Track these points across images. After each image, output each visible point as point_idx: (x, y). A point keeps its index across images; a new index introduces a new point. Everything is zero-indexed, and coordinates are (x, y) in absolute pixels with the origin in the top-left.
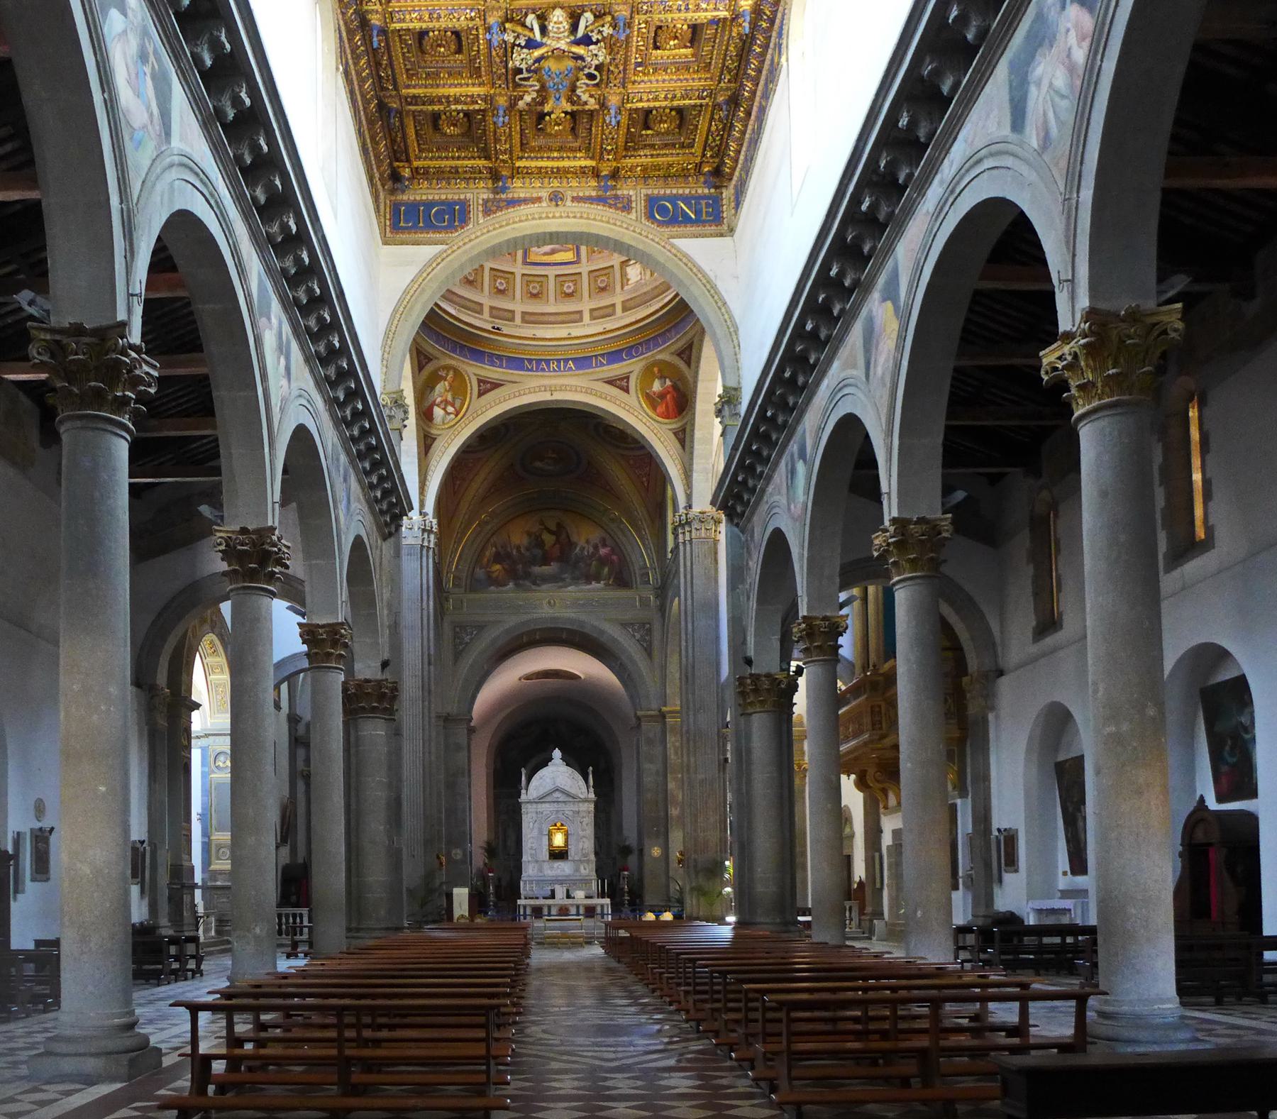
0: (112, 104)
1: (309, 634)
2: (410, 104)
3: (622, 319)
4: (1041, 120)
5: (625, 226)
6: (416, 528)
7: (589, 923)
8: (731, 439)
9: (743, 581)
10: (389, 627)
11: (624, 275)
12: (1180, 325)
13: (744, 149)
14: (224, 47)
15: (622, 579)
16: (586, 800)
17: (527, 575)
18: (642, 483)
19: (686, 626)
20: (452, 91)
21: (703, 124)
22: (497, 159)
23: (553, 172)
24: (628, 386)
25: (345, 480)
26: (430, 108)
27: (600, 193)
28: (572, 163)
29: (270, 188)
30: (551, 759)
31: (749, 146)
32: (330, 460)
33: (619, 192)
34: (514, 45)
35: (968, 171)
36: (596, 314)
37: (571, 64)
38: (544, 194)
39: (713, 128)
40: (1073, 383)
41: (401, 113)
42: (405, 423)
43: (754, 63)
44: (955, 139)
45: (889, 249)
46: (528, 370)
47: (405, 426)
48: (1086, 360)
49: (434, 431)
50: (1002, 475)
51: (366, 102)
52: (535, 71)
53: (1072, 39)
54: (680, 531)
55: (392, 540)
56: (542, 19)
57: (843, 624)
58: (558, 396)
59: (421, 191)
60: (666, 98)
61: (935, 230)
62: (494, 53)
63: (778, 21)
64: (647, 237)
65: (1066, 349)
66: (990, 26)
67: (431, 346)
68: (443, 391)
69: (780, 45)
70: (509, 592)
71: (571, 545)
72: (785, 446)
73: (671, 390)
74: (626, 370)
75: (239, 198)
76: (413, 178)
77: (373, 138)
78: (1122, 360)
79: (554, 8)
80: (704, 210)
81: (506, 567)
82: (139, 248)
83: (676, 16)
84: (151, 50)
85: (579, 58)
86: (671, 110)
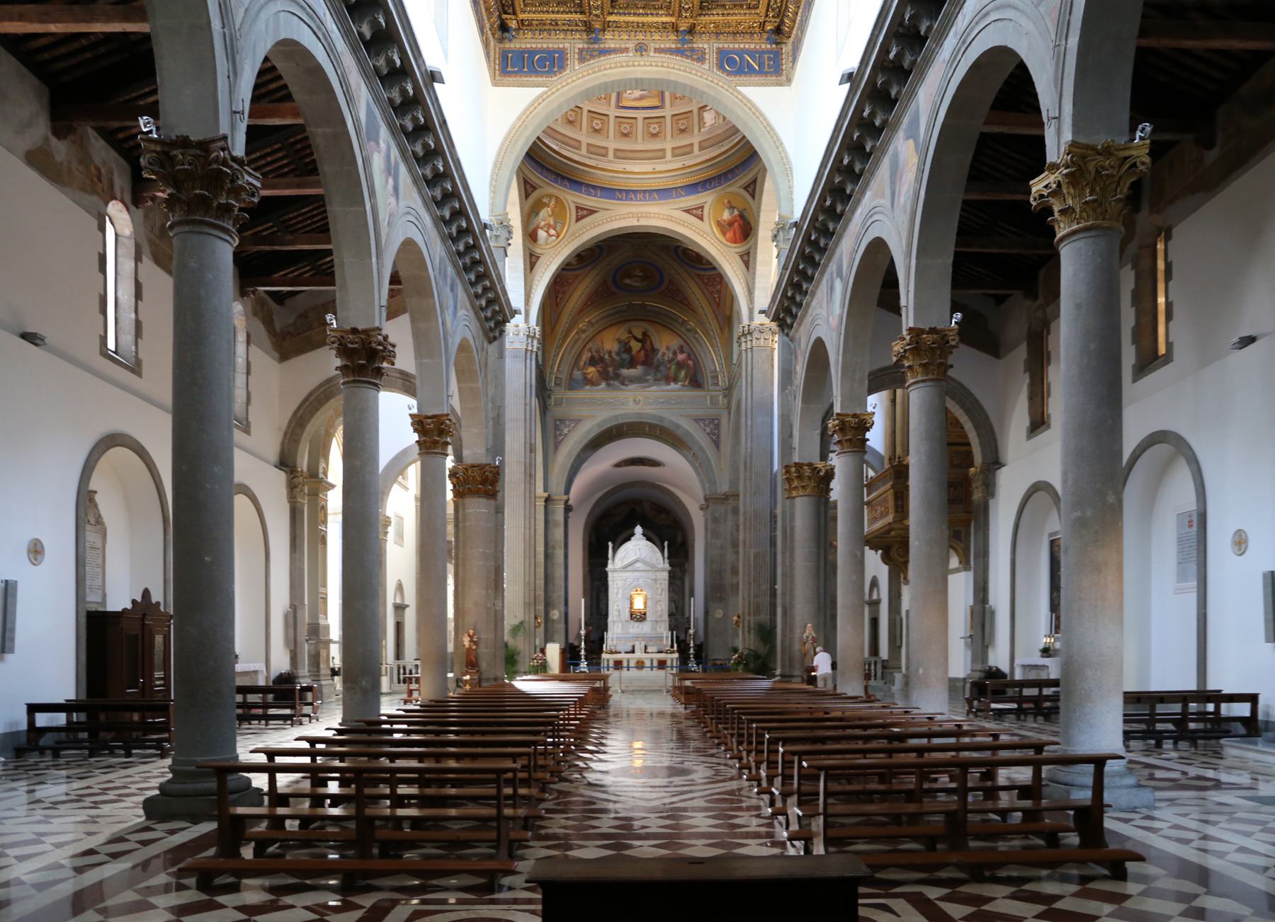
3: (699, 156)
5: (699, 74)
6: (522, 334)
7: (662, 673)
8: (783, 260)
10: (493, 419)
11: (701, 119)
12: (1147, 160)
15: (696, 382)
16: (663, 570)
17: (617, 376)
18: (714, 298)
19: (746, 422)
23: (638, 27)
24: (702, 215)
28: (655, 19)
29: (375, 24)
30: (633, 535)
31: (804, 9)
32: (437, 272)
33: (695, 45)
35: (977, 23)
38: (631, 45)
40: (1056, 209)
42: (510, 242)
45: (912, 93)
46: (619, 199)
47: (510, 244)
48: (1068, 188)
49: (538, 251)
50: (1007, 296)
54: (743, 339)
55: (496, 343)
57: (870, 421)
58: (643, 222)
59: (526, 40)
61: (950, 75)
64: (718, 84)
67: (535, 177)
68: (546, 215)
70: (601, 392)
71: (654, 350)
72: (826, 266)
73: (738, 218)
74: (703, 201)
75: (346, 33)
76: (520, 29)
78: (1098, 188)
80: (767, 63)
81: (600, 369)
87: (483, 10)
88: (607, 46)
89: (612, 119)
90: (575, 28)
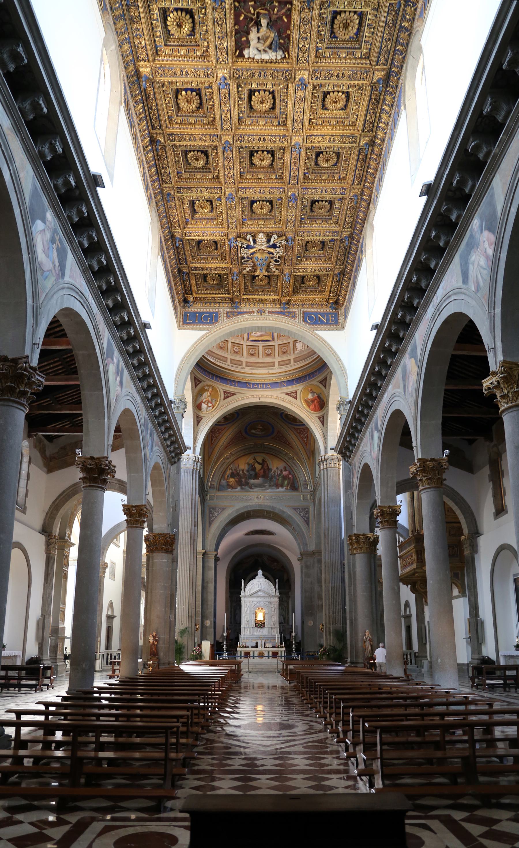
0: (33, 259)
1: (127, 510)
2: (193, 270)
3: (293, 366)
4: (475, 279)
7: (275, 660)
9: (351, 488)
10: (172, 507)
11: (294, 346)
13: (348, 293)
14: (94, 239)
15: (294, 487)
17: (247, 484)
20: (213, 266)
21: (329, 282)
22: (233, 294)
23: (259, 301)
25: (151, 435)
26: (202, 272)
27: (282, 310)
28: (268, 297)
30: (257, 575)
31: (350, 292)
32: (142, 426)
34: (241, 247)
35: (444, 301)
36: (281, 363)
37: (267, 255)
38: (255, 310)
39: (334, 284)
40: (498, 395)
41: (189, 274)
43: (351, 257)
44: (438, 287)
45: (412, 335)
46: (248, 388)
48: (504, 384)
49: (202, 415)
51: (173, 270)
52: (251, 258)
53: (486, 245)
54: (321, 464)
55: (176, 465)
56: (254, 237)
58: (263, 400)
60: (311, 271)
62: (232, 250)
63: (361, 241)
65: (494, 379)
66: (450, 240)
67: (200, 375)
69: (362, 251)
70: (238, 492)
71: (269, 469)
73: (317, 398)
75: (99, 305)
77: (175, 284)
79: (259, 233)
82: (41, 323)
83: (315, 237)
84: (57, 239)
85: (271, 253)
86: (314, 276)
87: (175, 293)
88: (242, 310)
90: (224, 301)
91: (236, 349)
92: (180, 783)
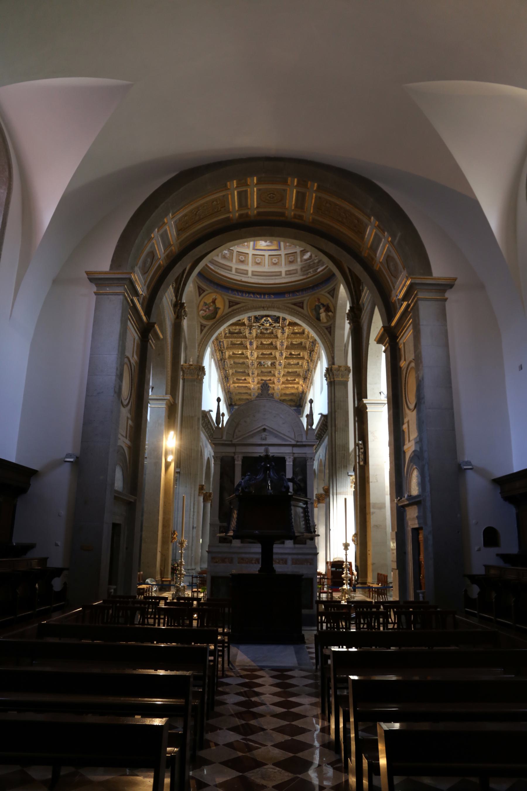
24: (201, 294)
89: (250, 256)
91: (242, 258)
92: (211, 722)
